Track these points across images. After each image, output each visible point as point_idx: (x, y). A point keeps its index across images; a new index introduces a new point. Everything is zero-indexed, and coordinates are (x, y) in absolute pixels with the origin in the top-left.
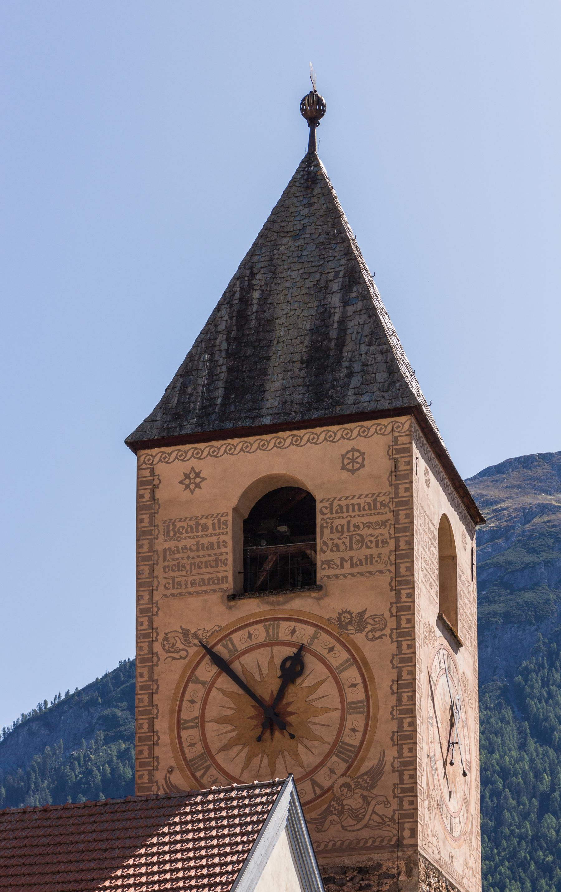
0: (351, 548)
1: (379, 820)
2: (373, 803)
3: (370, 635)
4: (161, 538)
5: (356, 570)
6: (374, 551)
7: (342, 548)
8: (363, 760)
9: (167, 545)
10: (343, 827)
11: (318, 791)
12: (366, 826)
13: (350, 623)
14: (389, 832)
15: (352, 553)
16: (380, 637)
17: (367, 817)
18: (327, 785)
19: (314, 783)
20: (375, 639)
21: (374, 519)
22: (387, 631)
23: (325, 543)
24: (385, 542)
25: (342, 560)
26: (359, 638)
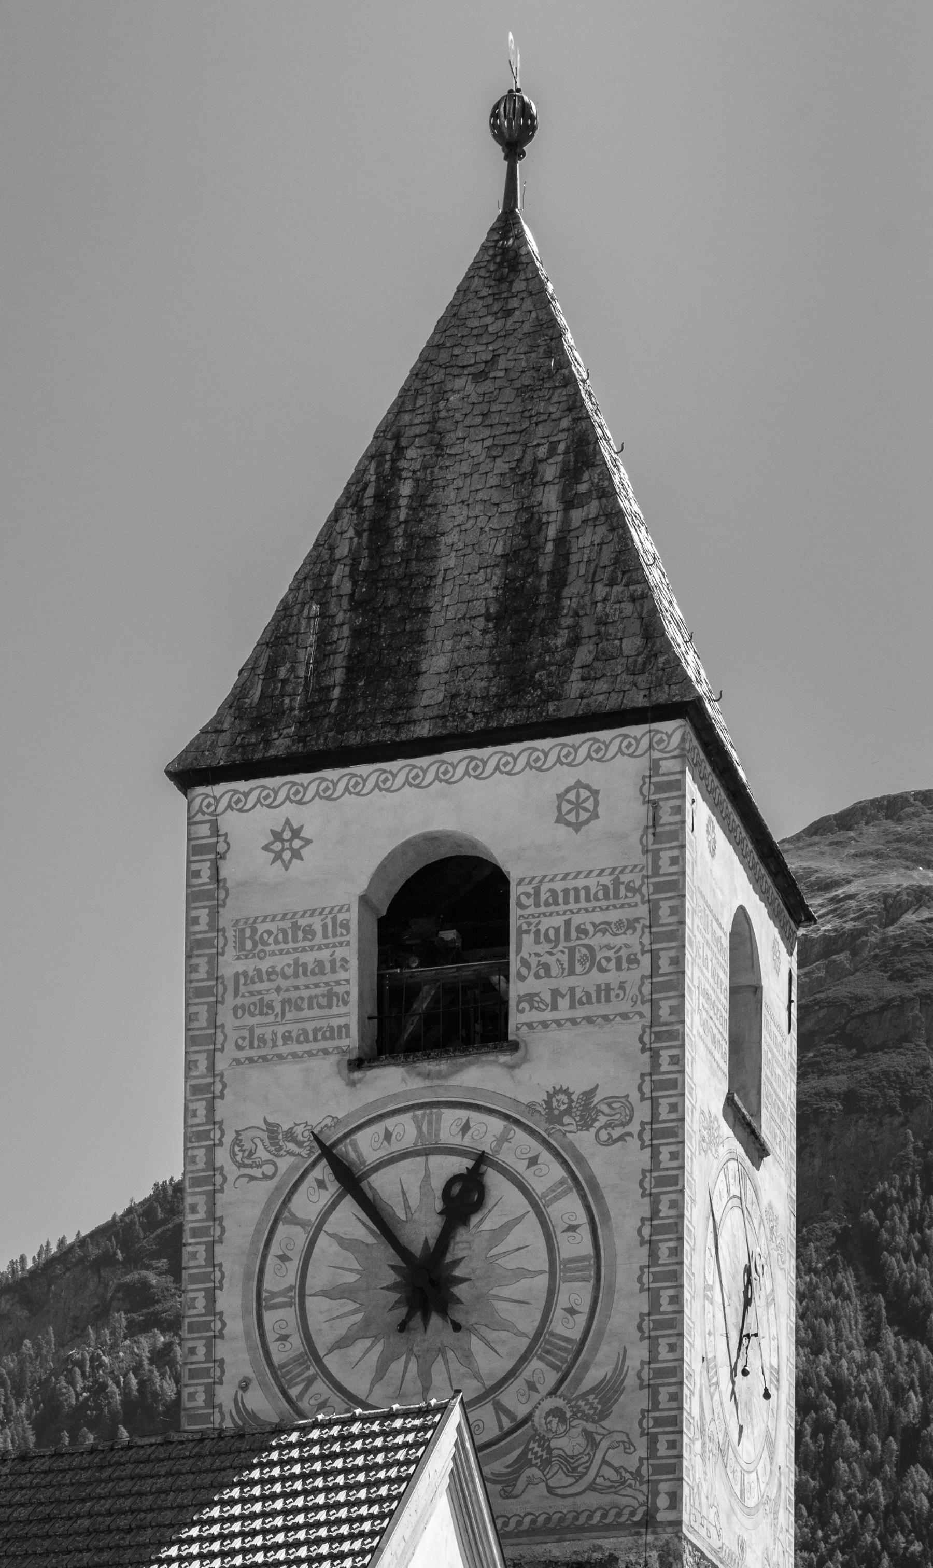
0: (572, 972)
1: (614, 1476)
2: (604, 1444)
3: (604, 1135)
4: (230, 952)
5: (580, 1012)
6: (612, 977)
7: (555, 970)
8: (586, 1367)
9: (240, 966)
10: (550, 1490)
11: (507, 1424)
12: (592, 1487)
13: (568, 1111)
14: (632, 1499)
15: (572, 981)
16: (621, 1138)
17: (592, 1472)
18: (521, 1411)
19: (499, 1408)
20: (612, 1141)
21: (613, 916)
22: (634, 1128)
23: (525, 963)
24: (633, 961)
25: (556, 993)
26: (584, 1140)
